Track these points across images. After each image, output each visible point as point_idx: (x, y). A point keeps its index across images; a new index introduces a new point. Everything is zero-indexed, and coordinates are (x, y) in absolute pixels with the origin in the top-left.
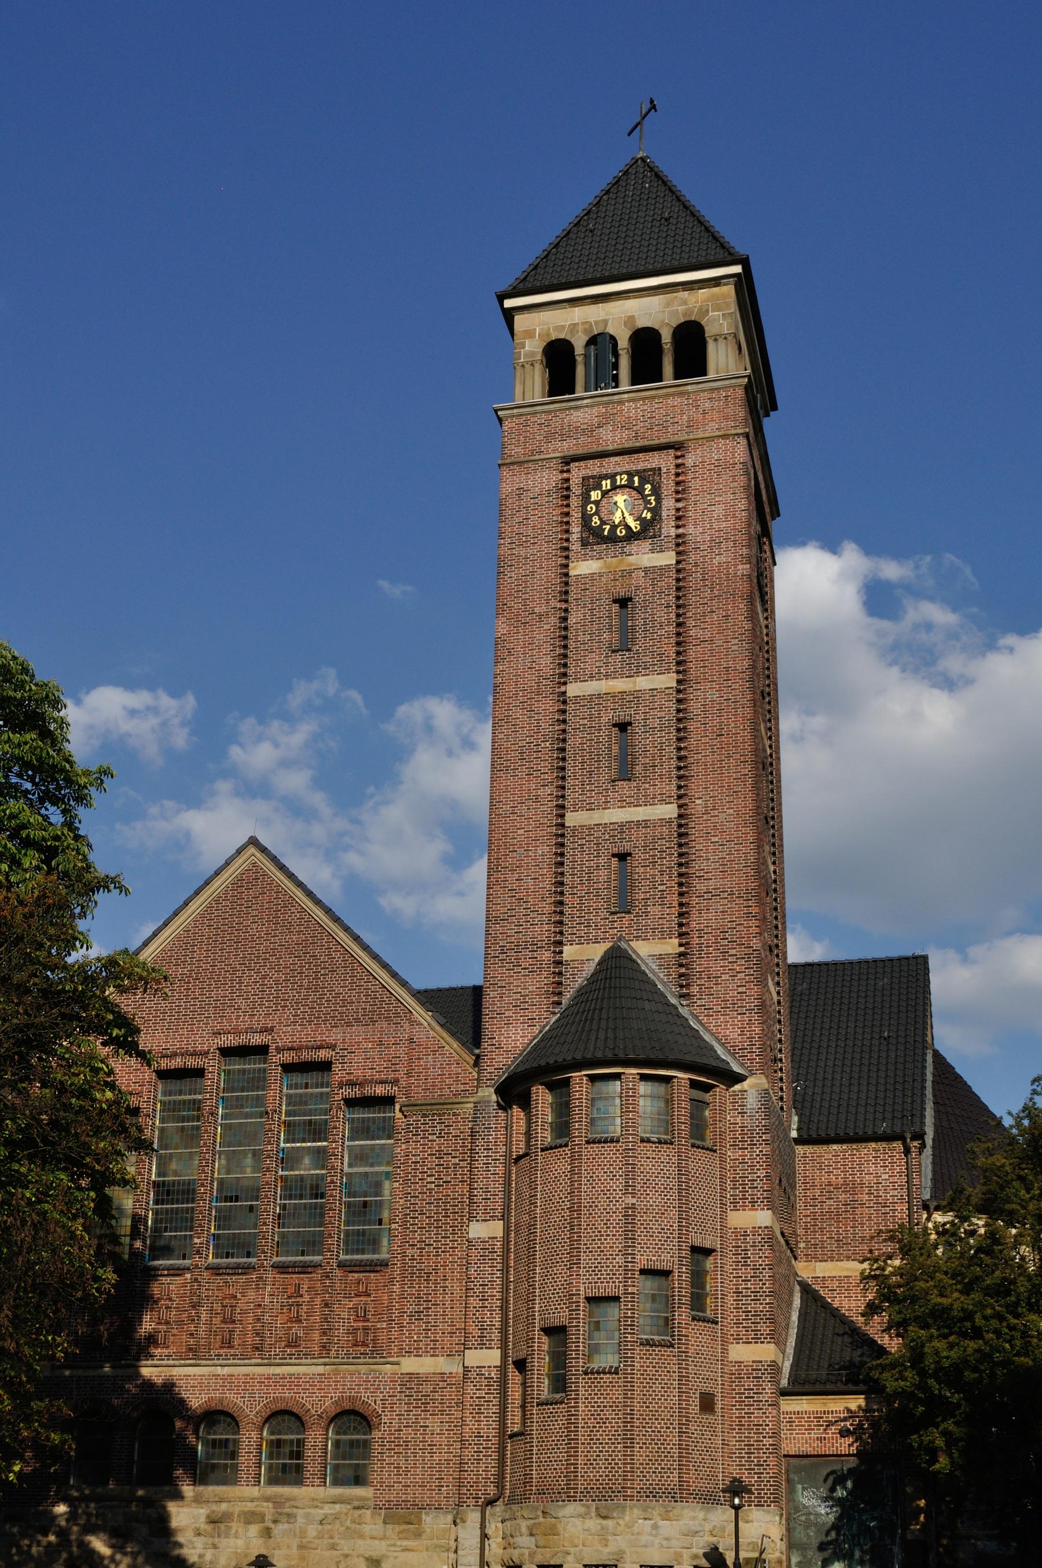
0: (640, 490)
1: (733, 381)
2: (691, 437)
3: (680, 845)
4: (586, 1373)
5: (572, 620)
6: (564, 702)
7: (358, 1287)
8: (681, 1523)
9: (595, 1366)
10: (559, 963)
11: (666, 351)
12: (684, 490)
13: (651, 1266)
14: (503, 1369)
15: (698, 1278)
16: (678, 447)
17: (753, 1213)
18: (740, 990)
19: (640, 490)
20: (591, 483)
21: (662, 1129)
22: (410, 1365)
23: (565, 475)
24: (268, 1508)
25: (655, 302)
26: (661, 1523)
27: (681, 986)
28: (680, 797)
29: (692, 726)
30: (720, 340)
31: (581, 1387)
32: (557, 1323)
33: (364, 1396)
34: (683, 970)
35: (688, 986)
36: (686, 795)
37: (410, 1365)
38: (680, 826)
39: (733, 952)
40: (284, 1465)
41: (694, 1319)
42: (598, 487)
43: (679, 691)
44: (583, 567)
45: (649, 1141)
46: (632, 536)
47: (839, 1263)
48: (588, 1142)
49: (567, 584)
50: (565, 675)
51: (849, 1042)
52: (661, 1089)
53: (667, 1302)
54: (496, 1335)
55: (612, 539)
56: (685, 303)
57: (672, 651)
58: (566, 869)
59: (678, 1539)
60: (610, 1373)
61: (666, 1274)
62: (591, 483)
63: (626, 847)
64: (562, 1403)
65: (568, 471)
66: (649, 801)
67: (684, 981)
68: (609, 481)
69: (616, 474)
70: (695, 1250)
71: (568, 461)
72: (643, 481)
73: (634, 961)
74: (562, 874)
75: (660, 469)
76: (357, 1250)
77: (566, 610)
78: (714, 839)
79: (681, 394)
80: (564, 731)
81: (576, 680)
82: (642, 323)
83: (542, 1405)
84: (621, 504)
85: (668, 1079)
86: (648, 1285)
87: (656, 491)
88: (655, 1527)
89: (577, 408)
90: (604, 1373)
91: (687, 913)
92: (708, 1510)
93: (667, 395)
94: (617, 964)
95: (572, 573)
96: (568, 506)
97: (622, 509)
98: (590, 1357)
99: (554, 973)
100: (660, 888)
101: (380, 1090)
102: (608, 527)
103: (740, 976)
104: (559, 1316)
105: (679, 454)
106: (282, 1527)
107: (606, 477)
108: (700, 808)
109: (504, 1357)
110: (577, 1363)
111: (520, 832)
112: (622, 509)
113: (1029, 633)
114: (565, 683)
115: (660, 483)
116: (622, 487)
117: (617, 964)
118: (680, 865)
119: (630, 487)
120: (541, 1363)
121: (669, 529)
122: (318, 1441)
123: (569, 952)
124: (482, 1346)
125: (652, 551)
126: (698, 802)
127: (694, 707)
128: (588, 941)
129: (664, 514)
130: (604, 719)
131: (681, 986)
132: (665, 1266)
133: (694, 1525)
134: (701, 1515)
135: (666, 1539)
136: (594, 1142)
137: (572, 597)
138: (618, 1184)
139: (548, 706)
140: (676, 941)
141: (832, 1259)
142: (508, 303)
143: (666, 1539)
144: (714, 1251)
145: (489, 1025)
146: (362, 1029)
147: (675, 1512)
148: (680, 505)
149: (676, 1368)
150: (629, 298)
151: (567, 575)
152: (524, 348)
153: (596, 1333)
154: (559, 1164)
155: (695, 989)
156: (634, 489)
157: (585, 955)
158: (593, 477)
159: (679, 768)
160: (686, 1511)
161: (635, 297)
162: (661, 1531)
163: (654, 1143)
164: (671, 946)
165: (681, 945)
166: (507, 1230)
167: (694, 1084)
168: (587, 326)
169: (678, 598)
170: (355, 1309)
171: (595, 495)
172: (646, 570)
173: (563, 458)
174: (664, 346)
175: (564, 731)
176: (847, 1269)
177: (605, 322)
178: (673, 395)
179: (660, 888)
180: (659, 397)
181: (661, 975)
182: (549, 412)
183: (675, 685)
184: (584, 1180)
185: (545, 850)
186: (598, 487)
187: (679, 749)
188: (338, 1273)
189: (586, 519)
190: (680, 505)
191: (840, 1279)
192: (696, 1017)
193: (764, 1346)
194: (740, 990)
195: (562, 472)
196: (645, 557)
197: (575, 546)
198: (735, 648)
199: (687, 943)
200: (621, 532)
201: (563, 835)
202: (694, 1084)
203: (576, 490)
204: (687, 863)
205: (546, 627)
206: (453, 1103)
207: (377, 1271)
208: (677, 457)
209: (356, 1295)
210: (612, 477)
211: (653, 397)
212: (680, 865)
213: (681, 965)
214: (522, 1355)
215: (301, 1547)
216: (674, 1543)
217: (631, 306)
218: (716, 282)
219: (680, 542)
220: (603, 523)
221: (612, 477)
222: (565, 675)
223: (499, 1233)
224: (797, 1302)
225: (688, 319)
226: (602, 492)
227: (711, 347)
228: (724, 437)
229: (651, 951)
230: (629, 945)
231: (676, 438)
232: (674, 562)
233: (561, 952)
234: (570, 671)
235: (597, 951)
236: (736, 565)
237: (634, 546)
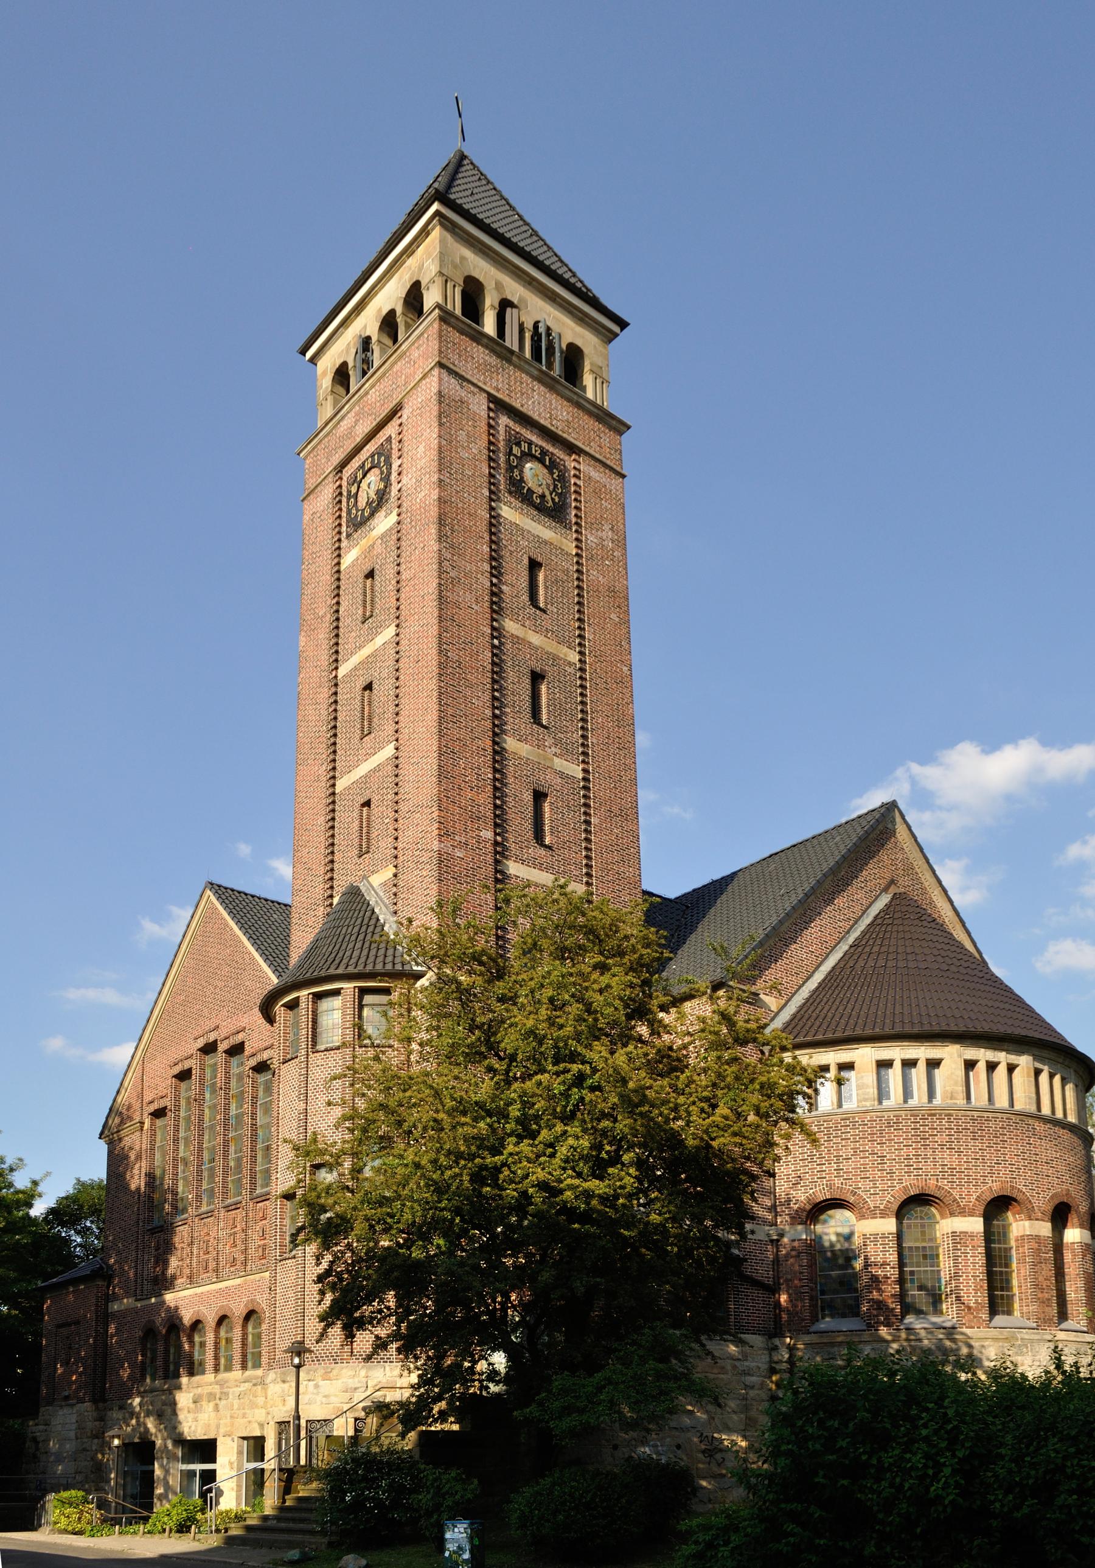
8: (340, 1381)
24: (216, 1389)
26: (321, 1383)
51: (977, 1002)
59: (336, 1396)
79: (400, 357)
88: (317, 1386)
89: (343, 418)
92: (369, 1369)
93: (392, 366)
106: (223, 1402)
113: (579, 372)
133: (352, 1383)
134: (363, 1373)
135: (325, 1396)
143: (325, 1396)
147: (335, 1372)
160: (344, 1371)
162: (322, 1390)
173: (335, 469)
178: (395, 363)
187: (494, 698)
211: (384, 374)
215: (231, 1417)
216: (333, 1399)
223: (894, 1229)
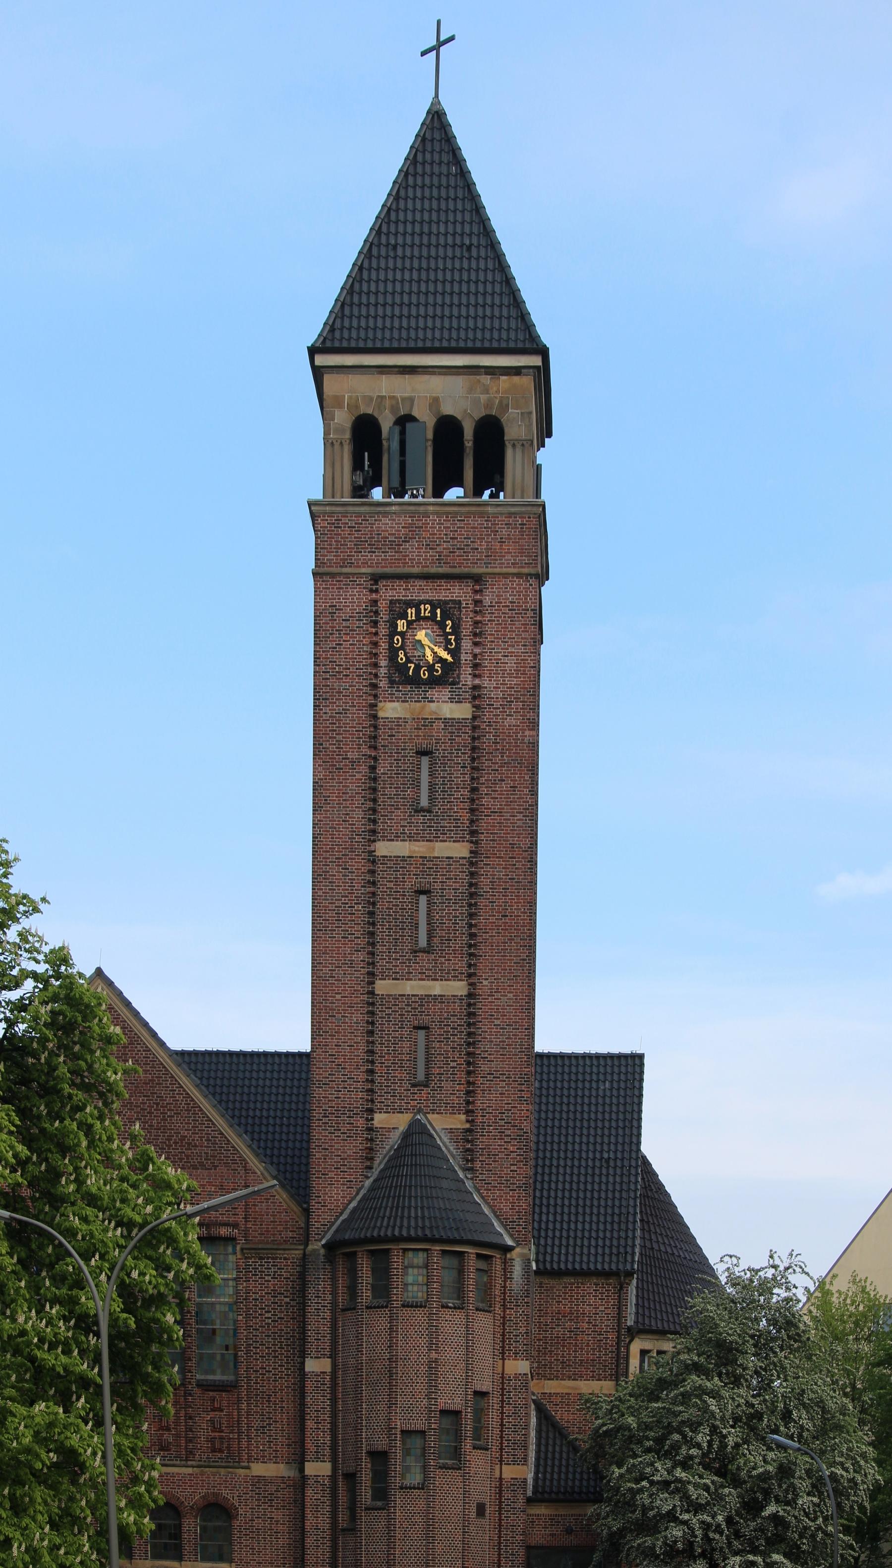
0: (442, 625)
1: (529, 509)
2: (489, 570)
3: (469, 1025)
4: (401, 1488)
5: (380, 770)
6: (374, 862)
7: (213, 1403)
9: (407, 1482)
10: (370, 1129)
11: (468, 450)
12: (481, 632)
13: (447, 1407)
14: (333, 1477)
15: (479, 1414)
16: (477, 579)
17: (516, 1362)
18: (513, 1168)
19: (442, 625)
20: (398, 610)
21: (455, 1295)
22: (258, 1469)
23: (374, 596)
25: (459, 383)
27: (467, 1161)
28: (470, 976)
29: (482, 902)
30: (518, 446)
31: (398, 1498)
32: (380, 1449)
33: (225, 1493)
34: (469, 1146)
35: (472, 1161)
36: (475, 974)
37: (258, 1469)
38: (469, 1005)
39: (508, 1132)
40: (166, 1544)
41: (474, 1448)
42: (404, 616)
43: (472, 864)
44: (390, 710)
45: (448, 1307)
46: (434, 682)
47: (563, 1382)
48: (403, 1306)
49: (375, 727)
50: (374, 832)
52: (455, 1262)
53: (458, 1436)
54: (327, 1451)
55: (415, 681)
56: (487, 391)
57: (466, 816)
58: (376, 1037)
60: (419, 1488)
61: (457, 1413)
62: (398, 610)
63: (425, 1020)
64: (384, 1509)
65: (377, 591)
66: (444, 976)
67: (469, 1156)
68: (414, 610)
69: (421, 602)
70: (476, 1393)
71: (376, 578)
72: (445, 615)
73: (431, 1136)
74: (373, 1042)
75: (460, 602)
76: (40, 1235)
77: (375, 759)
78: (497, 1022)
80: (374, 894)
81: (384, 838)
82: (447, 409)
83: (369, 1509)
84: (426, 641)
85: (462, 1253)
86: (447, 1422)
87: (456, 630)
90: (414, 1488)
91: (473, 1091)
94: (417, 1134)
95: (381, 714)
96: (376, 634)
97: (428, 645)
98: (403, 1477)
99: (367, 1139)
100: (452, 1064)
101: (224, 1231)
102: (413, 666)
103: (513, 1155)
104: (381, 1444)
105: (477, 587)
107: (409, 604)
108: (486, 989)
109: (335, 1469)
110: (396, 1480)
111: (338, 997)
112: (428, 645)
114: (374, 841)
115: (460, 619)
116: (425, 618)
117: (417, 1134)
118: (469, 1044)
119: (432, 621)
120: (365, 1478)
121: (466, 678)
122: (191, 1526)
123: (379, 1119)
124: (317, 1459)
125: (451, 700)
126: (485, 983)
127: (484, 882)
128: (394, 1111)
129: (463, 657)
130: (408, 885)
131: (467, 1161)
132: (457, 1407)
136: (408, 1306)
137: (381, 742)
138: (423, 1342)
139: (359, 865)
140: (463, 1117)
141: (557, 1378)
142: (320, 360)
144: (488, 1393)
145: (317, 1183)
146: (206, 1172)
148: (477, 650)
149: (461, 1485)
150: (434, 373)
151: (375, 717)
152: (333, 420)
153: (408, 1458)
154: (380, 1321)
155: (478, 1165)
156: (437, 622)
157: (393, 1122)
158: (399, 601)
159: (470, 946)
161: (440, 374)
163: (451, 1308)
164: (459, 1121)
165: (468, 1121)
166: (334, 1366)
167: (479, 1256)
168: (394, 402)
169: (473, 759)
170: (212, 1421)
171: (401, 625)
172: (446, 721)
174: (466, 443)
175: (374, 894)
176: (569, 1387)
177: (411, 400)
179: (452, 1064)
180: (461, 514)
181: (451, 1148)
182: (358, 515)
183: (467, 855)
184: (400, 1337)
185: (358, 1017)
186: (404, 616)
188: (197, 1391)
189: (393, 653)
190: (477, 650)
191: (562, 1395)
192: (478, 1191)
193: (520, 1467)
194: (513, 1168)
195: (371, 591)
196: (448, 708)
197: (383, 683)
198: (519, 823)
199: (473, 1121)
200: (424, 675)
201: (373, 1004)
202: (479, 1256)
203: (384, 616)
204: (474, 1043)
205: (358, 776)
206: (284, 1250)
207: (228, 1391)
208: (476, 592)
209: (212, 1410)
210: (417, 605)
212: (469, 1044)
213: (468, 1141)
214: (351, 1470)
217: (434, 385)
218: (517, 371)
219: (476, 695)
220: (408, 660)
221: (417, 605)
222: (374, 832)
223: (328, 1369)
224: (533, 1420)
225: (488, 413)
226: (408, 622)
227: (509, 453)
228: (519, 575)
229: (444, 1125)
230: (427, 1118)
231: (476, 570)
232: (470, 717)
233: (372, 1119)
234: (380, 827)
235: (401, 1121)
236: (523, 730)
237: (434, 693)
